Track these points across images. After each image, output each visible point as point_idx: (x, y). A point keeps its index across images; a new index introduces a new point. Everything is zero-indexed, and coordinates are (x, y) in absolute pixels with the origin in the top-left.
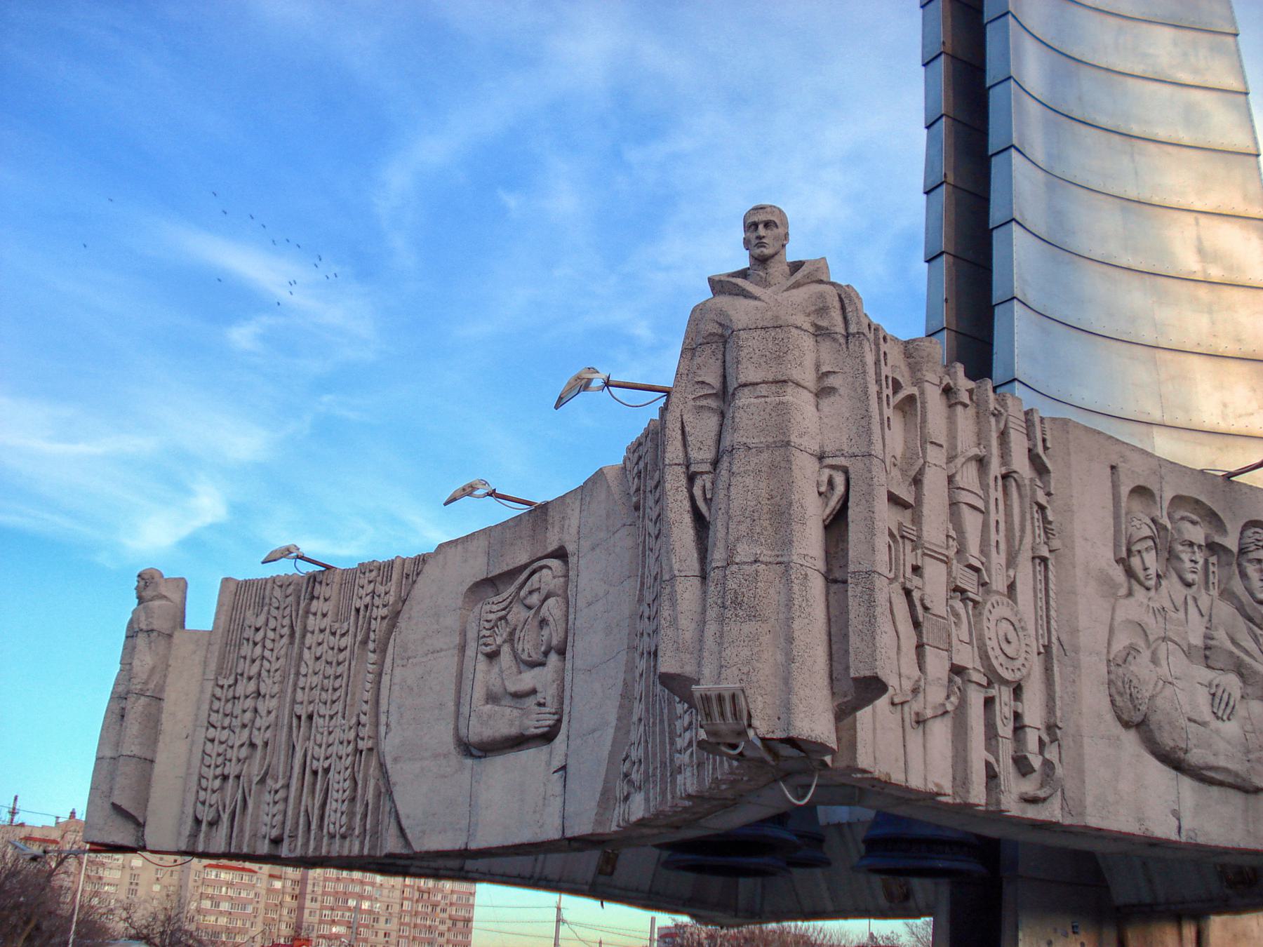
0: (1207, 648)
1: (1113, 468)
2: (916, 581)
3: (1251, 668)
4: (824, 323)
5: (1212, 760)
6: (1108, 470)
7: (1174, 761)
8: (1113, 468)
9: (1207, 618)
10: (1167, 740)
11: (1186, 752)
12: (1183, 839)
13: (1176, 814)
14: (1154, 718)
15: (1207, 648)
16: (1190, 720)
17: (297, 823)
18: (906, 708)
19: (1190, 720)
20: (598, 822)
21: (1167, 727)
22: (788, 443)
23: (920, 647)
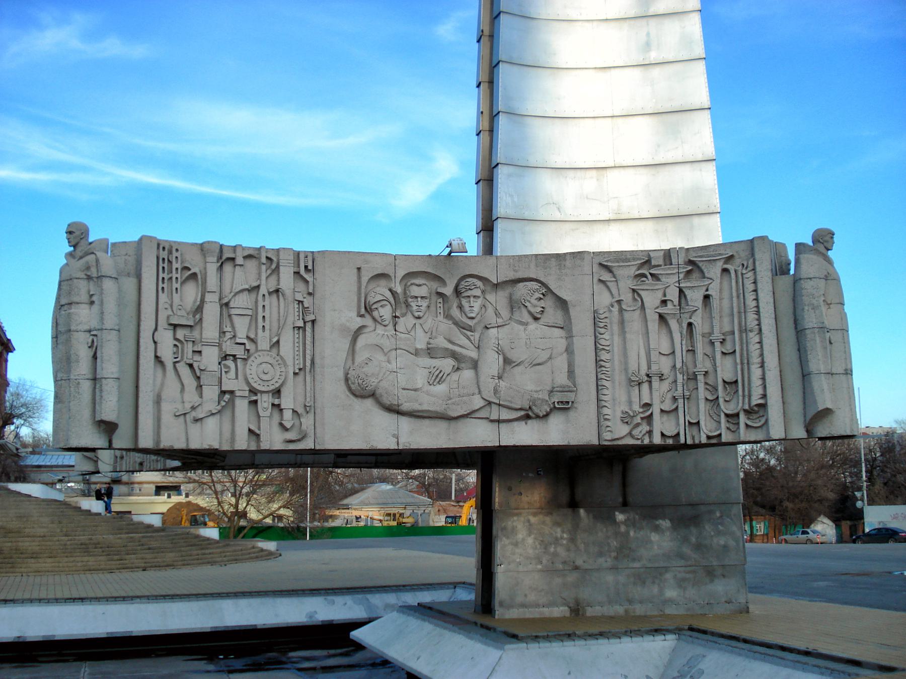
0: (428, 349)
1: (359, 269)
2: (197, 357)
3: (461, 354)
4: (89, 273)
5: (420, 408)
6: (356, 270)
7: (394, 410)
8: (359, 269)
9: (429, 333)
10: (386, 401)
11: (398, 406)
12: (401, 447)
13: (397, 437)
14: (378, 392)
15: (428, 349)
16: (404, 389)
17: (732, 308)
18: (188, 416)
19: (404, 389)
20: (248, 446)
21: (385, 395)
22: (70, 330)
23: (200, 387)
